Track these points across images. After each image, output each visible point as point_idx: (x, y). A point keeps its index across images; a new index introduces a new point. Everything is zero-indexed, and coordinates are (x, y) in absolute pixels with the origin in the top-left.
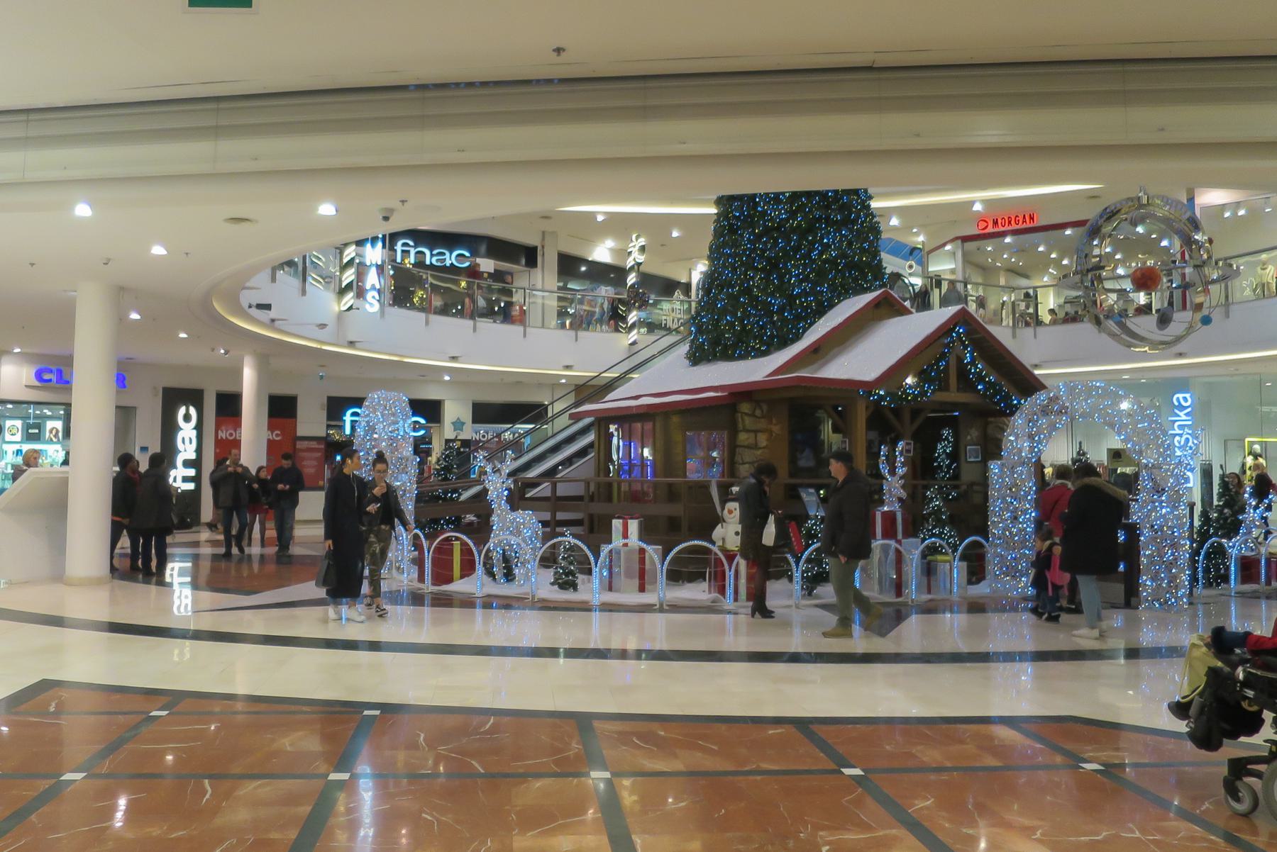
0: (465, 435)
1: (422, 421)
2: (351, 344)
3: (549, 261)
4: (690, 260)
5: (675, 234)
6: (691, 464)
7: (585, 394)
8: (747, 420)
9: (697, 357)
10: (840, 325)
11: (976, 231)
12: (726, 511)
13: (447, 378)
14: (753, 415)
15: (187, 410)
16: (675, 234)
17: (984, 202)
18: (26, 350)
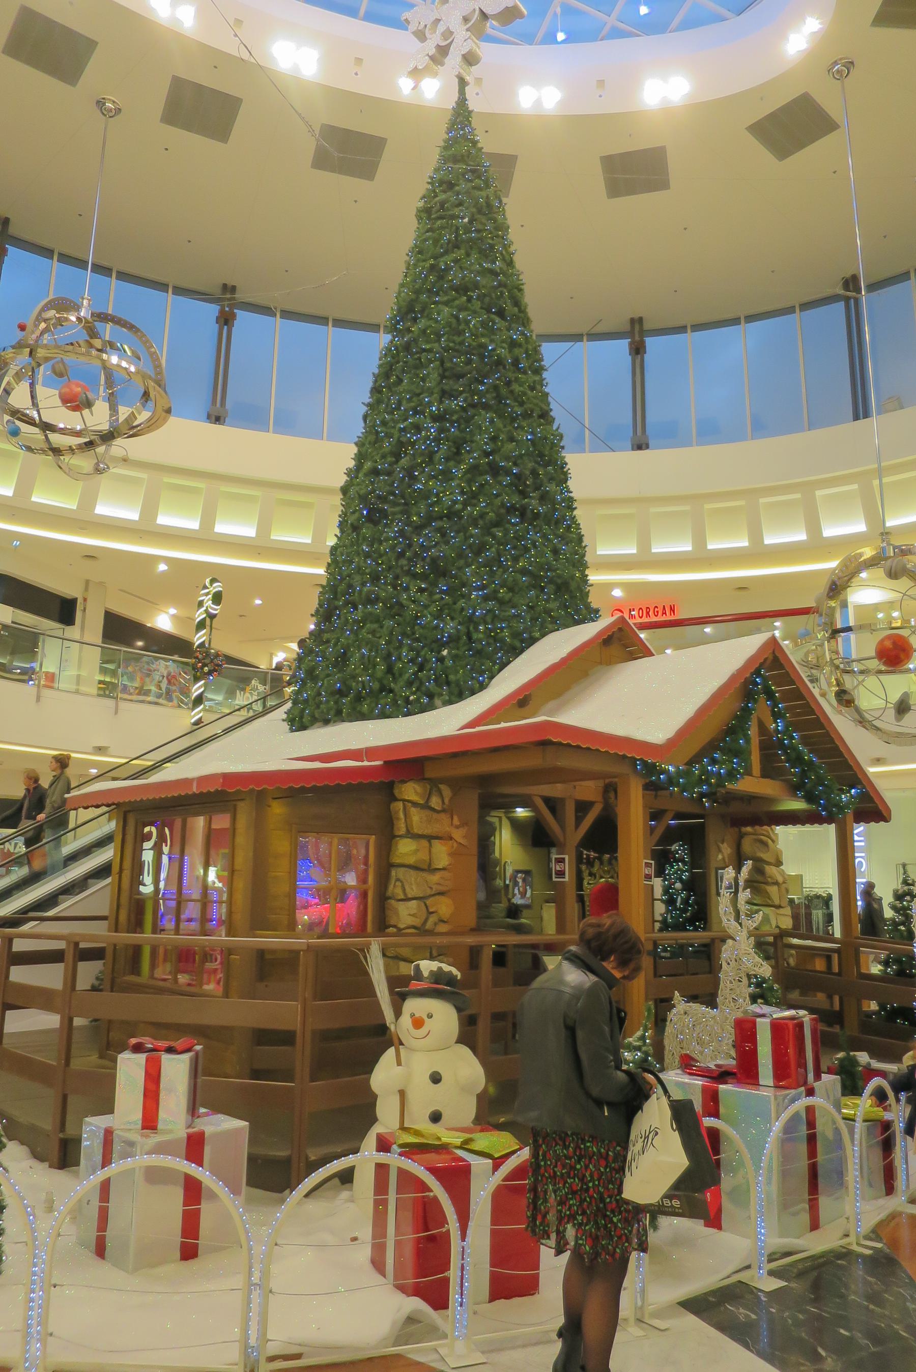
3: (90, 624)
4: (271, 640)
5: (258, 602)
8: (416, 816)
10: (564, 661)
12: (406, 1020)
14: (426, 806)
16: (258, 602)
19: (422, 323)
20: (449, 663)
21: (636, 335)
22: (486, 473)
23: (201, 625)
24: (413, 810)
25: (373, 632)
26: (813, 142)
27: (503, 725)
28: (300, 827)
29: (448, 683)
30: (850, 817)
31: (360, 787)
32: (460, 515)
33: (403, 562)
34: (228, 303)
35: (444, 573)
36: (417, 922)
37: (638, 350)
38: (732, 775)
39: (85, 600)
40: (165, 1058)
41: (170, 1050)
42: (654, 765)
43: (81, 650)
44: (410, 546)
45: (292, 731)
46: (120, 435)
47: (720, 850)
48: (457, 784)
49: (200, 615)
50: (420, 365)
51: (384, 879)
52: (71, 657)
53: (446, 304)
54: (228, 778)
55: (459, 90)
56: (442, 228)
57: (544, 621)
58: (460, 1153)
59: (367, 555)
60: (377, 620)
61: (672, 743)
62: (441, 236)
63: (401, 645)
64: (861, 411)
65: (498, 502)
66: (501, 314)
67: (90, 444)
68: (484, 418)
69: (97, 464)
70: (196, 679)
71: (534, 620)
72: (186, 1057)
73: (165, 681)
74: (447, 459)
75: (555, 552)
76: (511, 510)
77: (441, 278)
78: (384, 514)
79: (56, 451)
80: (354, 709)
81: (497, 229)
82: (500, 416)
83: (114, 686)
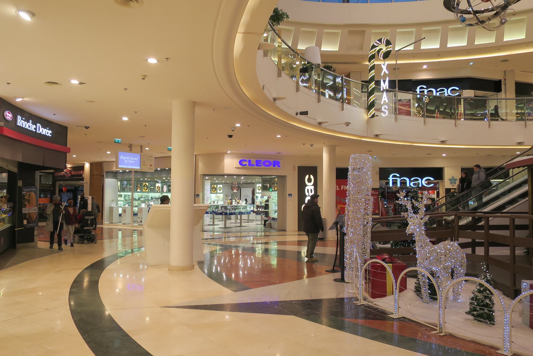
1: (432, 179)
2: (377, 136)
7: (500, 172)
15: (309, 177)
18: (232, 152)
26: (88, 343)
39: (505, 79)
43: (506, 102)
46: (510, 5)
55: (207, 306)
67: (496, 14)
69: (501, 21)
79: (482, 22)
83: (523, 114)
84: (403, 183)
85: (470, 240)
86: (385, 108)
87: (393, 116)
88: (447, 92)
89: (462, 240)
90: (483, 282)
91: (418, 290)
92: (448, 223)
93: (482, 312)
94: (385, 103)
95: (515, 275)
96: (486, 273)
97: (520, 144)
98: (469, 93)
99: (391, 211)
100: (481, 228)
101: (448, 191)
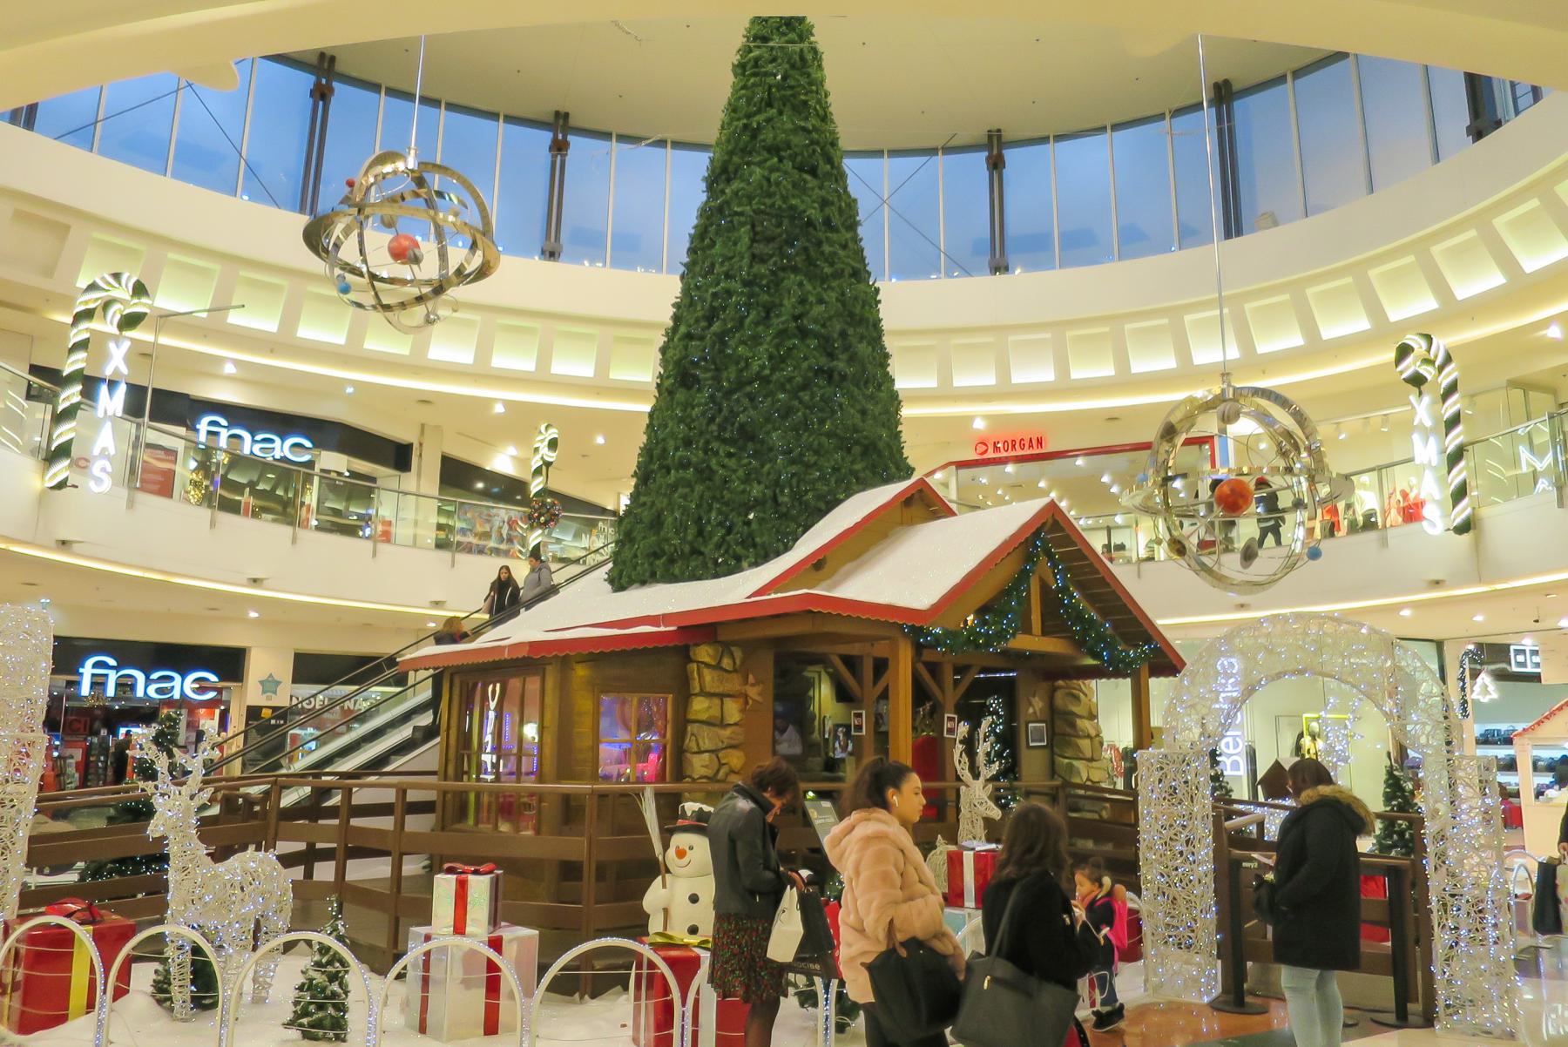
0: (281, 700)
1: (213, 678)
2: (64, 544)
3: (425, 475)
5: (600, 440)
6: (608, 751)
7: (388, 673)
8: (708, 676)
9: (619, 582)
10: (858, 525)
11: (972, 456)
12: (671, 852)
13: (253, 615)
14: (718, 667)
16: (600, 440)
17: (987, 417)
19: (736, 185)
20: (754, 526)
21: (995, 148)
22: (794, 336)
23: (538, 472)
24: (706, 672)
25: (685, 497)
27: (773, 596)
28: (600, 687)
29: (754, 545)
30: (1145, 670)
31: (656, 651)
32: (774, 378)
33: (714, 427)
34: (561, 128)
35: (753, 438)
36: (709, 772)
37: (996, 164)
38: (1001, 635)
40: (471, 877)
41: (476, 872)
42: (921, 628)
44: (720, 410)
45: (615, 591)
46: (451, 284)
47: (1030, 704)
48: (749, 647)
49: (536, 463)
50: (732, 228)
51: (680, 734)
52: (408, 505)
53: (759, 164)
54: (534, 645)
56: (754, 85)
57: (849, 482)
58: (697, 950)
59: (681, 420)
60: (689, 485)
61: (937, 608)
62: (754, 94)
63: (710, 509)
64: (1233, 226)
65: (805, 365)
66: (813, 172)
68: (792, 279)
69: (428, 315)
70: (532, 528)
71: (839, 482)
72: (488, 877)
73: (506, 527)
74: (757, 324)
75: (863, 412)
76: (819, 372)
77: (754, 136)
78: (697, 380)
80: (667, 571)
81: (811, 84)
82: (811, 278)
84: (125, 686)
85: (301, 846)
86: (103, 470)
87: (124, 492)
88: (282, 448)
89: (285, 847)
90: (331, 942)
91: (161, 989)
92: (250, 802)
93: (320, 1014)
94: (104, 454)
95: (397, 920)
96: (337, 919)
97: (437, 604)
98: (335, 462)
99: (71, 770)
100: (333, 812)
101: (253, 713)
